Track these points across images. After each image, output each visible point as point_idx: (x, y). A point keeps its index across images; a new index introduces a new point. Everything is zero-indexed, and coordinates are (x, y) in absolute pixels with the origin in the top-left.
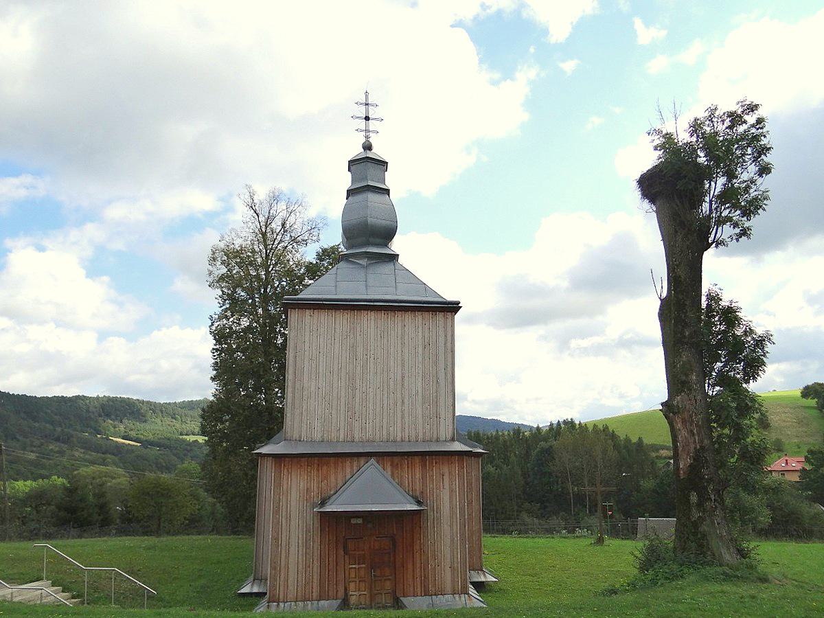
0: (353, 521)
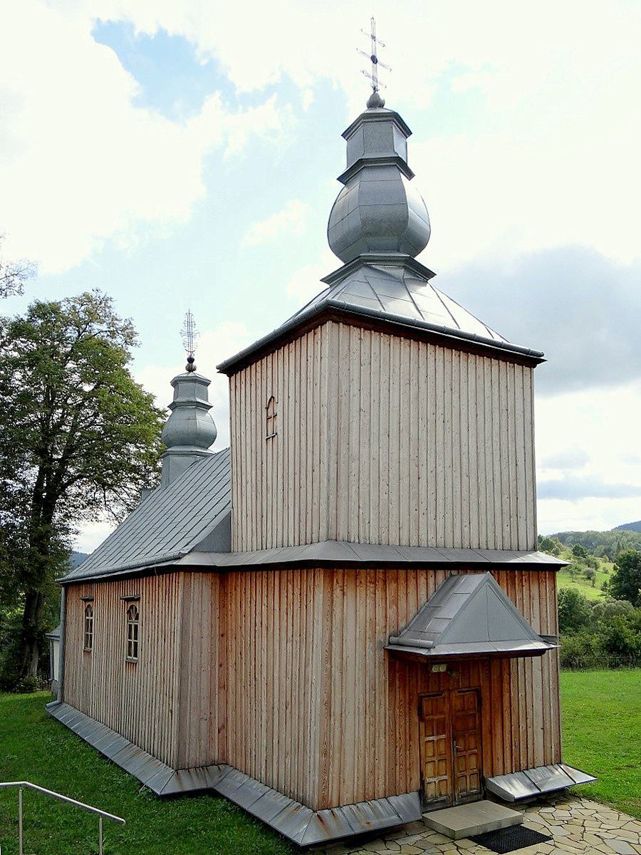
0: (435, 669)
